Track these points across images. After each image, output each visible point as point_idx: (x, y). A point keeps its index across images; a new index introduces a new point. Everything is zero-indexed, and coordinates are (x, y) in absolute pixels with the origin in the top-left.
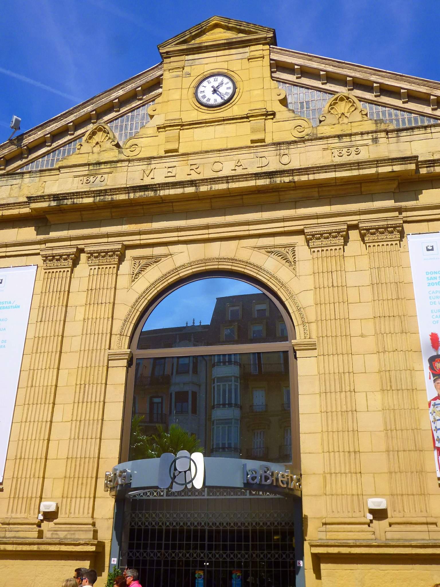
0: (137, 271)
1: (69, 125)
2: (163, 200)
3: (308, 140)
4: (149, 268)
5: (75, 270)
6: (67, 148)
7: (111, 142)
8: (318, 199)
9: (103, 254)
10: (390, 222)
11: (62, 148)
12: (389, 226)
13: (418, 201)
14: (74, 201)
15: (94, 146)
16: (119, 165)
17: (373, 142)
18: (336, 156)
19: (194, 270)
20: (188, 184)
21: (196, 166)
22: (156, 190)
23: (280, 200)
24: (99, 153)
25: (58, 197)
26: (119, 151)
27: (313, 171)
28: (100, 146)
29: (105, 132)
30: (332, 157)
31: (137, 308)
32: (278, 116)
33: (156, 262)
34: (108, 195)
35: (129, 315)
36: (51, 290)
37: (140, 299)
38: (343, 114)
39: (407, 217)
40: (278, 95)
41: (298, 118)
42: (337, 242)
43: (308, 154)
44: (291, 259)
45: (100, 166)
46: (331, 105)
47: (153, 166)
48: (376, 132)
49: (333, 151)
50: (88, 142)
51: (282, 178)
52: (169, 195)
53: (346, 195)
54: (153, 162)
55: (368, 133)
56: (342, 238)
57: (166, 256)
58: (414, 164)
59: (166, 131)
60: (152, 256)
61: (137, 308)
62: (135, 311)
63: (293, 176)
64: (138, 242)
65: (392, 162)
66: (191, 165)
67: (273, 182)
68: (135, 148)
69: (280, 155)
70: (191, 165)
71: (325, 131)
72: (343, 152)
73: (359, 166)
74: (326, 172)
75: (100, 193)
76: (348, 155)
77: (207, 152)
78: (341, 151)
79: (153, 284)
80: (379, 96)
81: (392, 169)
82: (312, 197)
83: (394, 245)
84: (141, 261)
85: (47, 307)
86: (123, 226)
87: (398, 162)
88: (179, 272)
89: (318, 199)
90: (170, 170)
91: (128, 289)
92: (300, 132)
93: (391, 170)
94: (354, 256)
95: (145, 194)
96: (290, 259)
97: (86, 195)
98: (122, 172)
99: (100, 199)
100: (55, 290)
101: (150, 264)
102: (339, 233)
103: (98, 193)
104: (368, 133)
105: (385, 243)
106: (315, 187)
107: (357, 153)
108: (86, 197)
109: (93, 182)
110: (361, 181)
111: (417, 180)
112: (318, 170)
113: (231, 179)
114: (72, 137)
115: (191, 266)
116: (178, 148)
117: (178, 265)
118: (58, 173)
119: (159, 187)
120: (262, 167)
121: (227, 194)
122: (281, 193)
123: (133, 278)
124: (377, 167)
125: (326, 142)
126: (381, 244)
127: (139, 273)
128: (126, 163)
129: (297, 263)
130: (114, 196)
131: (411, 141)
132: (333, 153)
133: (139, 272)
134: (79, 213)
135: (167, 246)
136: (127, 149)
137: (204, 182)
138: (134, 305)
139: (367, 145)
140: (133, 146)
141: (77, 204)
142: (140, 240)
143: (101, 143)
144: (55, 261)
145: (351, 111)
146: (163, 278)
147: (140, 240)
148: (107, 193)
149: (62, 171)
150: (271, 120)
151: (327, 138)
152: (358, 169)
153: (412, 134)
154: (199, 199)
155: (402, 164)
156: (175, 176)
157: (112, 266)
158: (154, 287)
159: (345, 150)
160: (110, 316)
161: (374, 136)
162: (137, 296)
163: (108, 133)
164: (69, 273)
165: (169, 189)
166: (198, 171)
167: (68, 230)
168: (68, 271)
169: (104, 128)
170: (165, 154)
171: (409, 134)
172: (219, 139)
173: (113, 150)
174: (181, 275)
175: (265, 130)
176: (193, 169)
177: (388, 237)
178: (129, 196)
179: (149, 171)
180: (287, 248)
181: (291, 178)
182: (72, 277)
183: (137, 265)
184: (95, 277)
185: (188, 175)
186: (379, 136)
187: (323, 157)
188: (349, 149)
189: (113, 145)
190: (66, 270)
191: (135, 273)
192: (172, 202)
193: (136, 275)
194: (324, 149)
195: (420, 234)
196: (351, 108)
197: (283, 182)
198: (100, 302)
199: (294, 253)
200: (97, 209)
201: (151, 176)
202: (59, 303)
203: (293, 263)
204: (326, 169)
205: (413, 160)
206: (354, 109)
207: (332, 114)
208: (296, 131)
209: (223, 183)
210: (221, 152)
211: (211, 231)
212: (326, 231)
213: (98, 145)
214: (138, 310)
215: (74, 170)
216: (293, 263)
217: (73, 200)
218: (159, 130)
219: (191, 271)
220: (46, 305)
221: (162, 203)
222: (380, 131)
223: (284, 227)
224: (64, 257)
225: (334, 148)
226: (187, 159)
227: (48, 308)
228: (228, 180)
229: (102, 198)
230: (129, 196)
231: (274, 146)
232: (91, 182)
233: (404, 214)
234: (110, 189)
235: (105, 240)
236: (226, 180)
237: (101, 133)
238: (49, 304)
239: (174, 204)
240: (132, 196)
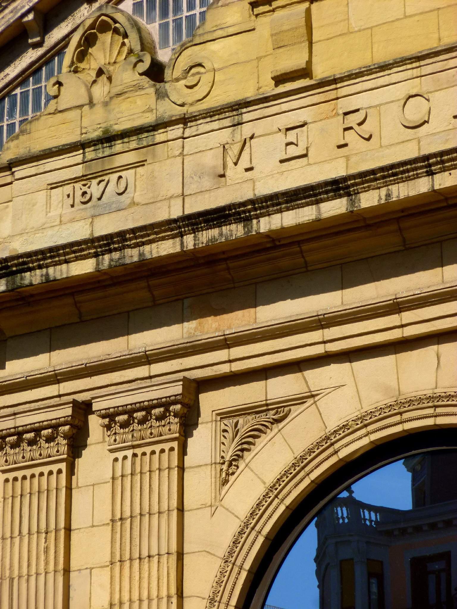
0: (230, 454)
1: (26, 19)
2: (273, 240)
4: (263, 439)
5: (81, 463)
6: (31, 87)
7: (135, 65)
9: (139, 415)
11: (18, 91)
14: (47, 274)
15: (94, 82)
16: (160, 136)
19: (374, 437)
20: (327, 192)
21: (358, 117)
22: (247, 220)
24: (106, 104)
25: (7, 267)
26: (157, 92)
28: (110, 79)
29: (116, 31)
31: (238, 563)
33: (278, 421)
34: (129, 247)
35: (219, 583)
36: (25, 531)
37: (245, 536)
45: (110, 146)
47: (246, 130)
50: (76, 71)
52: (283, 228)
54: (246, 117)
57: (300, 400)
59: (273, 11)
60: (267, 405)
61: (238, 563)
62: (236, 569)
64: (225, 369)
66: (346, 114)
68: (197, 77)
70: (346, 114)
75: (108, 244)
77: (384, 67)
79: (272, 487)
84: (241, 421)
85: (20, 577)
86: (186, 324)
88: (337, 446)
90: (292, 136)
91: (213, 509)
95: (221, 234)
97: (74, 252)
98: (168, 157)
99: (111, 260)
100: (34, 529)
101: (245, 446)
103: (105, 245)
108: (77, 259)
109: (99, 199)
113: (437, 163)
114: (40, 51)
115: (366, 426)
116: (309, 62)
117: (332, 426)
118: (9, 179)
119: (255, 209)
121: (439, 201)
123: (224, 475)
127: (238, 457)
128: (176, 131)
130: (147, 249)
133: (237, 455)
134: (69, 300)
135: (300, 371)
136: (177, 80)
137: (367, 182)
138: (231, 553)
140: (194, 71)
141: (55, 280)
142: (230, 361)
143: (111, 68)
144: (24, 445)
146: (298, 469)
147: (230, 361)
148: (126, 240)
149: (20, 172)
154: (368, 227)
156: (305, 156)
157: (166, 446)
158: (276, 496)
160: (173, 590)
162: (234, 526)
163: (126, 36)
164: (64, 475)
165: (280, 211)
166: (365, 129)
167: (50, 349)
168: (60, 471)
169: (115, 22)
170: (276, 85)
172: (416, 18)
173: (142, 88)
174: (342, 454)
176: (351, 128)
178: (182, 243)
179: (239, 145)
182: (74, 485)
183: (230, 435)
184: (128, 481)
185: (339, 147)
189: (141, 74)
190: (55, 468)
191: (228, 458)
192: (299, 243)
193: (230, 465)
198: (145, 553)
200: (114, 285)
201: (244, 163)
202: (47, 563)
209: (417, 176)
210: (422, 63)
211: (408, 316)
213: (104, 78)
214: (241, 568)
215: (48, 167)
217: (44, 270)
218: (256, 11)
219: (365, 441)
220: (16, 573)
221: (275, 247)
224: (45, 432)
226: (332, 95)
227: (24, 580)
228: (430, 166)
229: (116, 255)
230: (182, 243)
232: (94, 199)
234: (133, 231)
235: (142, 371)
236: (426, 167)
237: (109, 34)
238: (25, 571)
239: (305, 247)
240: (189, 241)
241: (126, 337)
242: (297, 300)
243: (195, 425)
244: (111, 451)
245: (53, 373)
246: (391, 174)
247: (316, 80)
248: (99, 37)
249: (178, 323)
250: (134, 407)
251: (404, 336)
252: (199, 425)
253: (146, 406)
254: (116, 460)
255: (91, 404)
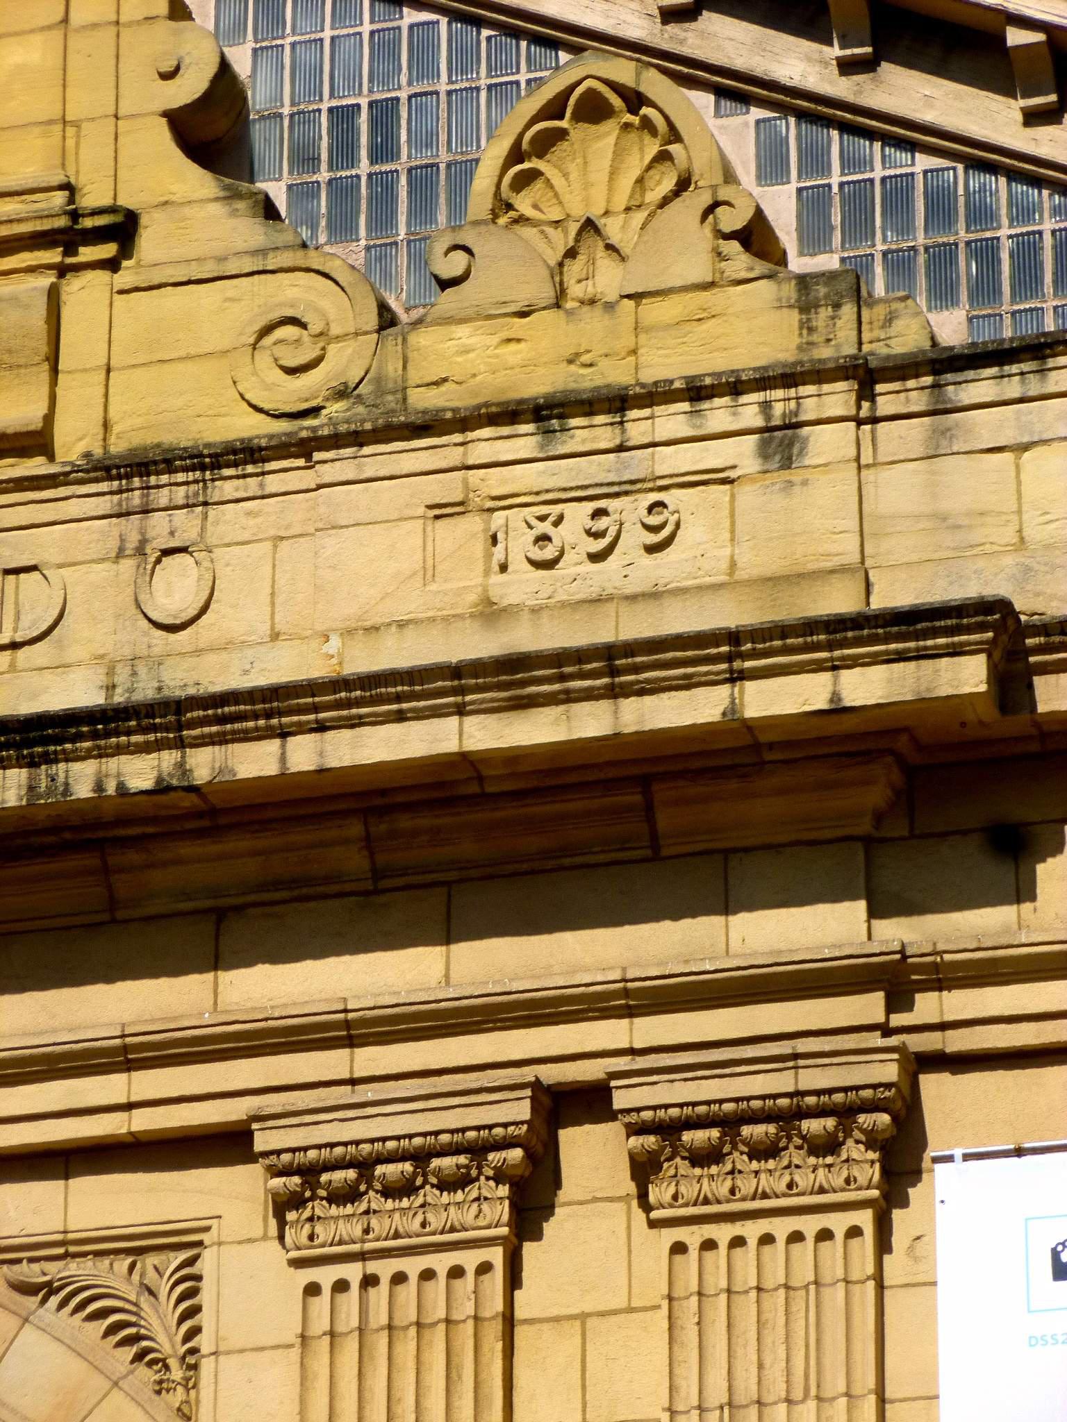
3: (336, 441)
8: (367, 893)
10: (813, 1078)
12: (811, 1100)
13: (1027, 907)
17: (764, 452)
18: (518, 564)
23: (113, 903)
27: (316, 708)
30: (487, 573)
32: (148, 243)
38: (589, 226)
39: (943, 1026)
40: (167, 76)
41: (285, 259)
42: (469, 1216)
43: (331, 543)
44: (166, 1340)
46: (516, 155)
48: (789, 378)
49: (499, 518)
51: (113, 764)
53: (550, 864)
55: (735, 387)
56: (504, 1190)
58: (982, 658)
63: (181, 744)
65: (830, 646)
67: (50, 792)
69: (140, 551)
71: (457, 367)
72: (560, 535)
73: (613, 672)
74: (400, 717)
76: (596, 557)
78: (545, 527)
80: (864, 66)
81: (835, 697)
82: (328, 879)
83: (839, 1235)
87: (886, 639)
89: (367, 893)
92: (291, 371)
93: (821, 704)
94: (583, 1317)
96: (162, 1338)
102: (478, 1151)
104: (735, 387)
105: (781, 1227)
106: (345, 814)
107: (654, 539)
110: (647, 769)
111: (1034, 747)
112: (349, 704)
116: (49, 419)
120: (14, 646)
122: (117, 859)
124: (736, 677)
125: (453, 456)
126: (752, 1230)
129: (207, 1366)
131: (1026, 447)
132: (494, 540)
139: (722, 478)
145: (654, 195)
150: (102, 276)
151: (464, 422)
152: (614, 693)
153: (1034, 386)
155: (901, 657)
159: (578, 514)
161: (778, 409)
171: (1013, 388)
175: (53, 359)
177: (803, 1179)
180: (152, 1260)
181: (168, 759)
186: (810, 410)
187: (428, 573)
188: (599, 513)
194: (441, 511)
195: (1019, 1152)
196: (655, 174)
197: (111, 789)
199: (192, 1293)
203: (177, 1373)
204: (399, 698)
205: (969, 630)
206: (668, 184)
207: (521, 220)
208: (263, 360)
212: (391, 1145)
216: (177, 1373)
222: (820, 375)
223: (129, 1106)
225: (504, 502)
231: (104, 486)
233: (927, 1007)
241: (210, 976)
242: (346, 958)
243: (548, 1210)
244: (298, 1263)
245: (118, 1041)
246: (368, 699)
247: (64, 464)
248: (217, 190)
249: (200, 971)
250: (433, 1141)
251: (133, 1129)
252: (557, 1210)
253: (779, 1109)
254: (312, 1290)
255: (250, 1134)
